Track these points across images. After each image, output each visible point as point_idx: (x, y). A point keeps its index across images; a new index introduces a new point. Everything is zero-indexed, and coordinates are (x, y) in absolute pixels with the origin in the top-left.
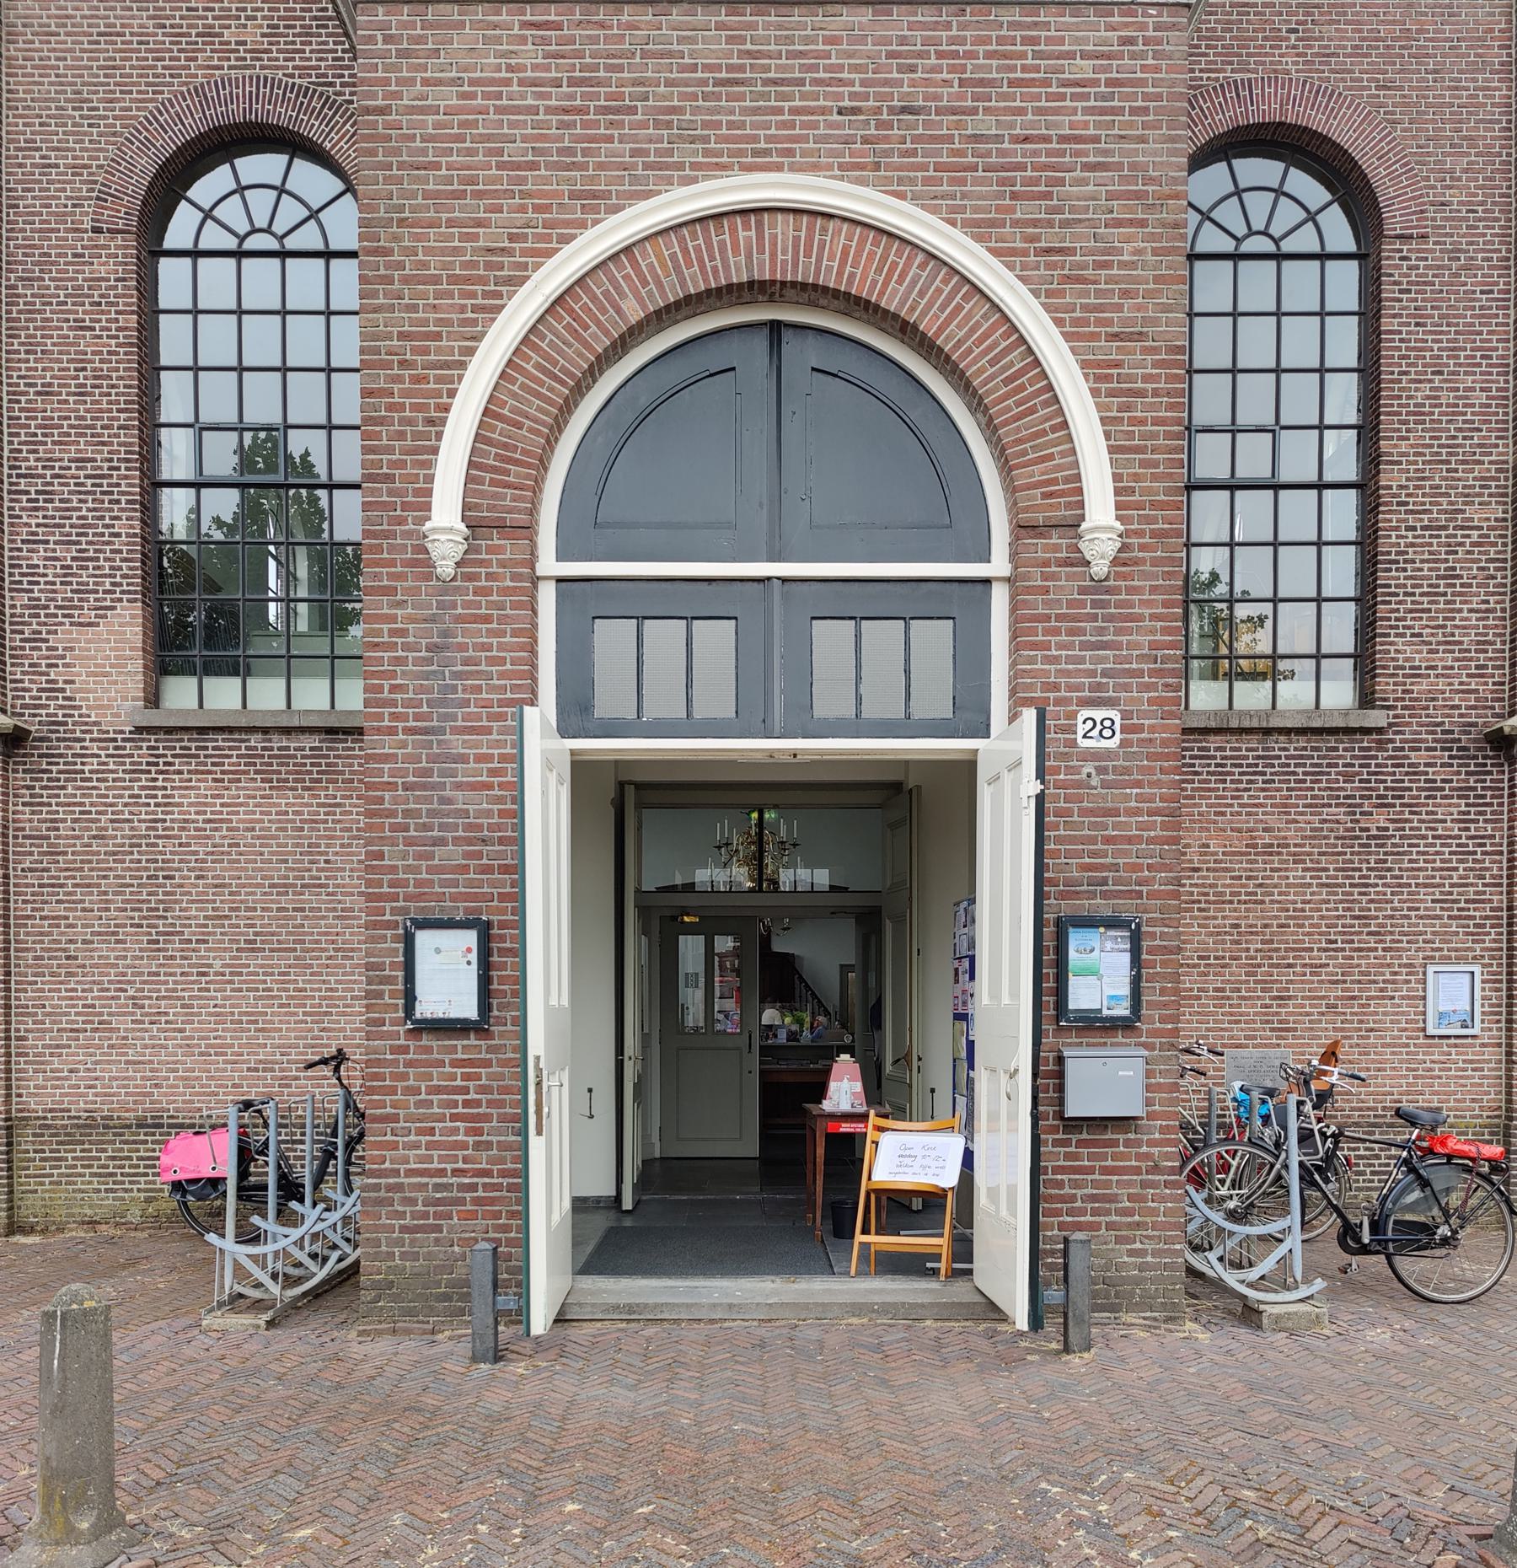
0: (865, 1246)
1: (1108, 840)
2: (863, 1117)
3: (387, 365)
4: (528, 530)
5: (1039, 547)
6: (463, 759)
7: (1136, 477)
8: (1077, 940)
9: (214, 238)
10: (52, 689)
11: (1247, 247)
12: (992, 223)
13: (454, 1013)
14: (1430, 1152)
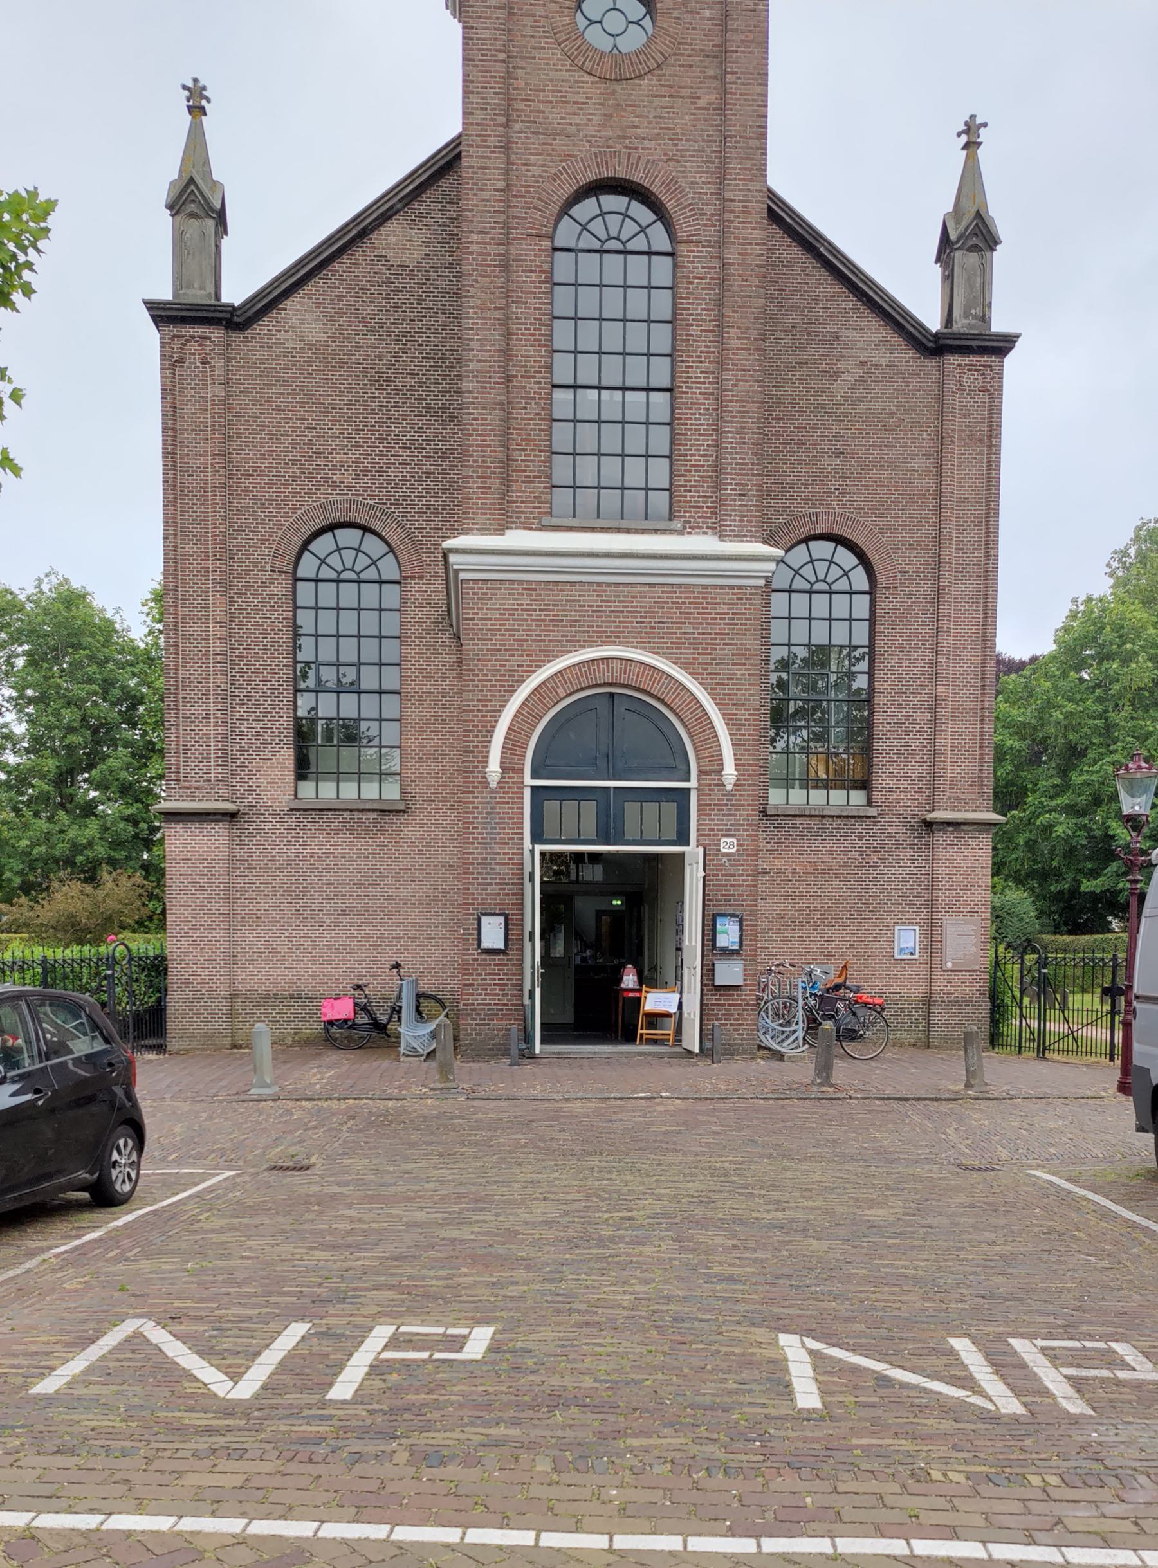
0: (642, 1035)
1: (731, 885)
2: (640, 991)
3: (473, 711)
5: (707, 779)
6: (499, 854)
7: (742, 755)
8: (719, 921)
9: (326, 573)
10: (250, 790)
11: (816, 587)
12: (690, 663)
13: (496, 946)
14: (857, 1002)
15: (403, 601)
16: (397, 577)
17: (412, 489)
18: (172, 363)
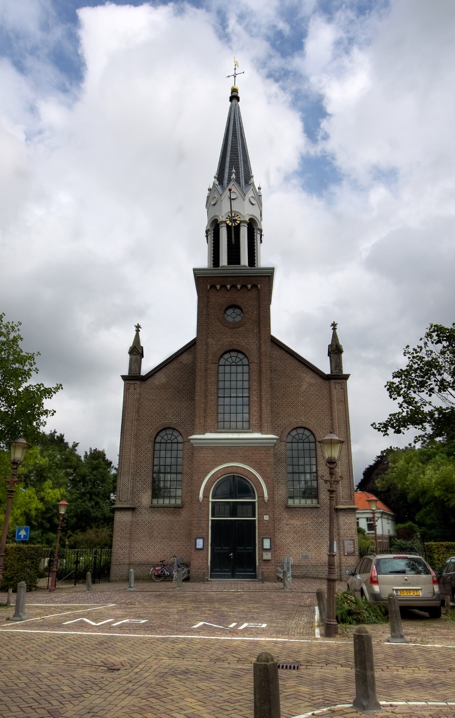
4: (209, 497)
15: (184, 448)
16: (182, 441)
17: (187, 418)
18: (126, 390)
